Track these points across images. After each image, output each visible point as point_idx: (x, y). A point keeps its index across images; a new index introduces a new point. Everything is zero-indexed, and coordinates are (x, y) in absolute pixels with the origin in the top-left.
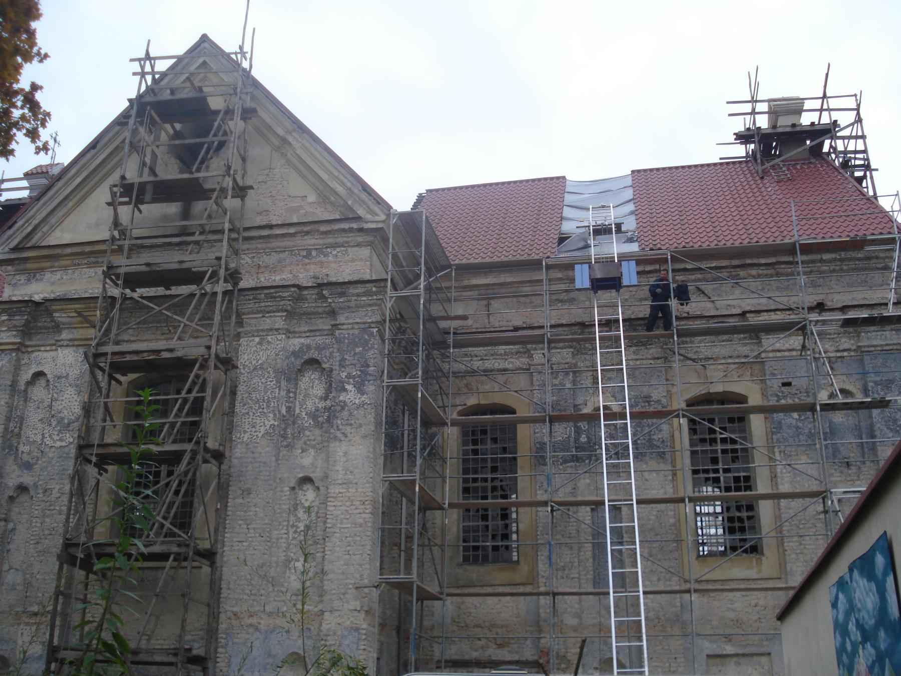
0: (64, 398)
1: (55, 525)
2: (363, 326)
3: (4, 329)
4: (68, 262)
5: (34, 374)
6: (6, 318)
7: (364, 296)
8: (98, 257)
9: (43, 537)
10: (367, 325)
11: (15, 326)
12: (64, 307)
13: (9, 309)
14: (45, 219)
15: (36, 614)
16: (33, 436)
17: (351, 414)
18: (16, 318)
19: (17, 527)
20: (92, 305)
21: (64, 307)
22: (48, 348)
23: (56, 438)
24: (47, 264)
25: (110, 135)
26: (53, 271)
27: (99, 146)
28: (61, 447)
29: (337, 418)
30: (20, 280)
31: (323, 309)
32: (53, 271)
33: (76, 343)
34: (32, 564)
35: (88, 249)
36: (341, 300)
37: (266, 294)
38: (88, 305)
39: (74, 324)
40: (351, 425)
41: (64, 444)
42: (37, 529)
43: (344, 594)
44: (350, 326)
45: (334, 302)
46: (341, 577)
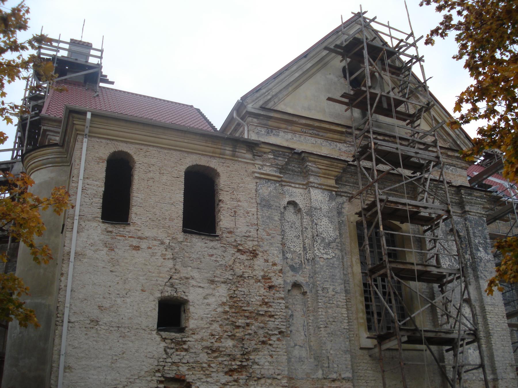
0: (322, 224)
1: (336, 315)
2: (480, 215)
3: (268, 164)
4: (299, 129)
5: (294, 201)
6: (272, 157)
7: (479, 198)
8: (319, 132)
9: (328, 323)
10: (481, 215)
11: (277, 164)
12: (317, 160)
13: (277, 151)
14: (276, 95)
15: (334, 380)
16: (292, 247)
17: (485, 265)
18: (280, 159)
19: (294, 314)
20: (335, 164)
21: (317, 160)
22: (297, 186)
23: (323, 252)
24: (283, 126)
25: (314, 53)
26: (285, 132)
27: (308, 57)
28: (327, 258)
29: (479, 266)
30: (261, 131)
31: (455, 200)
32: (285, 132)
33: (324, 187)
34: (325, 343)
35: (317, 124)
36: (469, 198)
37: (434, 184)
38: (333, 163)
39: (320, 173)
40: (487, 271)
41: (329, 257)
42: (323, 317)
43: (506, 369)
44: (474, 214)
45: (465, 198)
46: (503, 359)
